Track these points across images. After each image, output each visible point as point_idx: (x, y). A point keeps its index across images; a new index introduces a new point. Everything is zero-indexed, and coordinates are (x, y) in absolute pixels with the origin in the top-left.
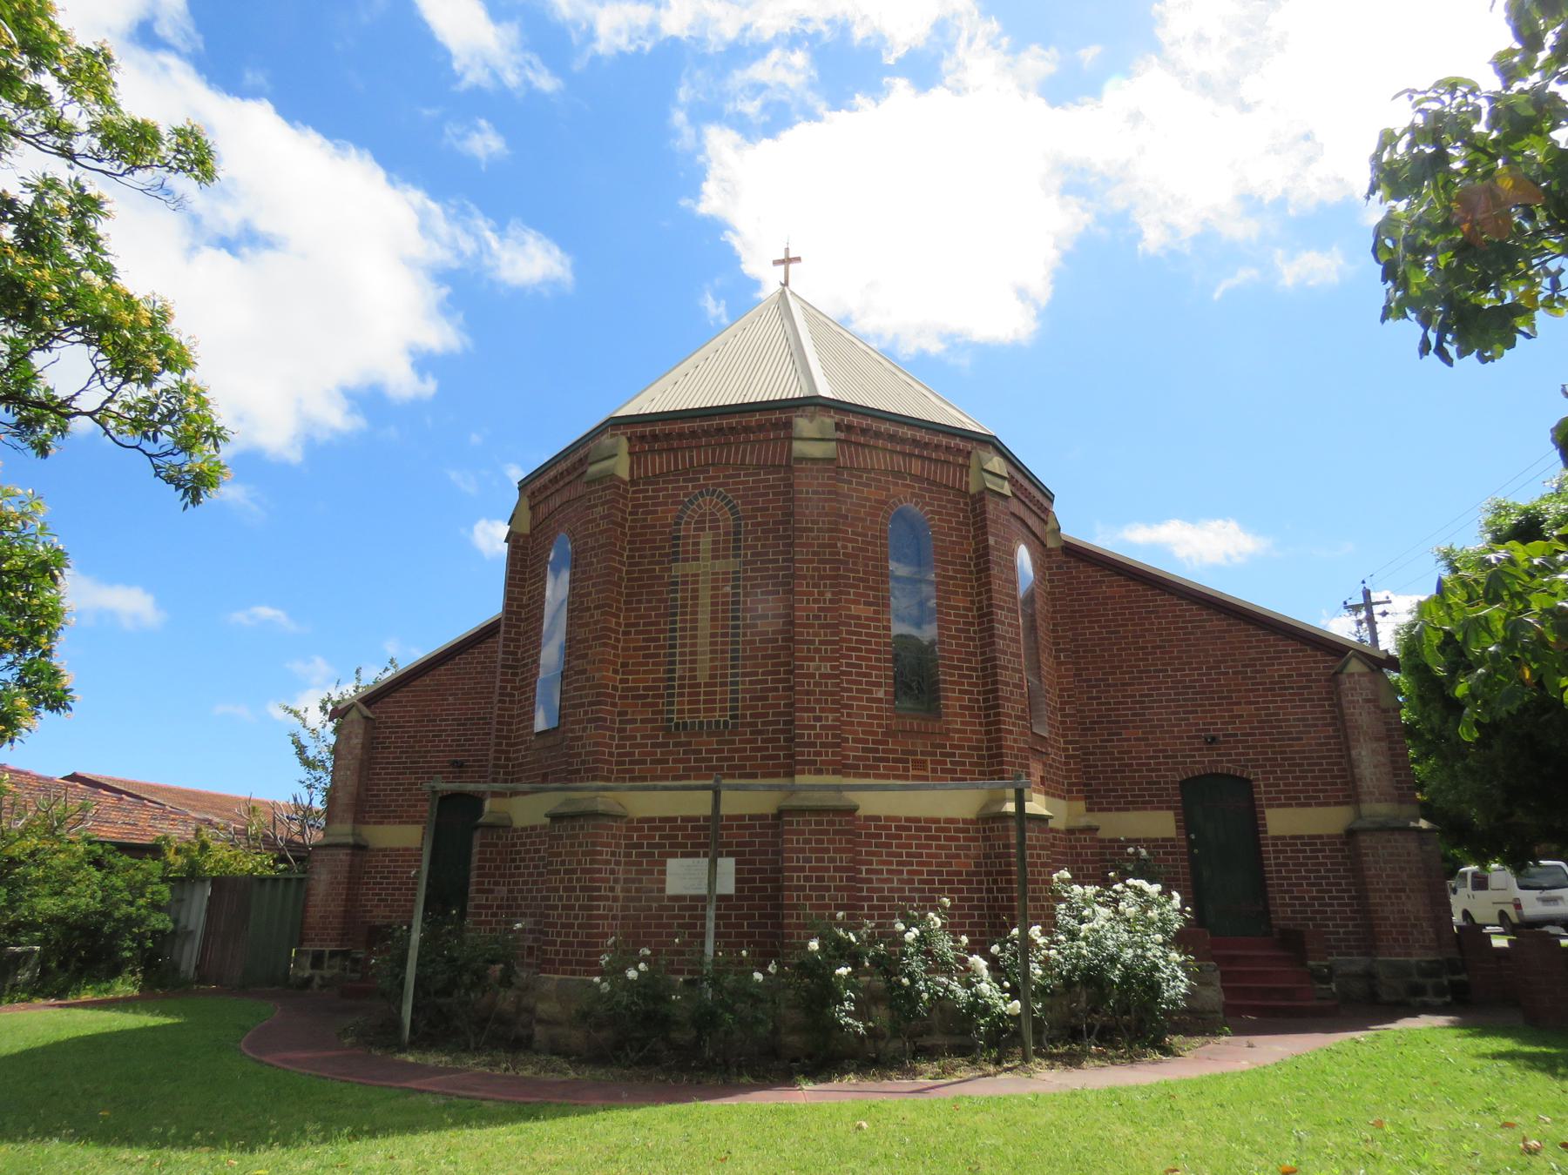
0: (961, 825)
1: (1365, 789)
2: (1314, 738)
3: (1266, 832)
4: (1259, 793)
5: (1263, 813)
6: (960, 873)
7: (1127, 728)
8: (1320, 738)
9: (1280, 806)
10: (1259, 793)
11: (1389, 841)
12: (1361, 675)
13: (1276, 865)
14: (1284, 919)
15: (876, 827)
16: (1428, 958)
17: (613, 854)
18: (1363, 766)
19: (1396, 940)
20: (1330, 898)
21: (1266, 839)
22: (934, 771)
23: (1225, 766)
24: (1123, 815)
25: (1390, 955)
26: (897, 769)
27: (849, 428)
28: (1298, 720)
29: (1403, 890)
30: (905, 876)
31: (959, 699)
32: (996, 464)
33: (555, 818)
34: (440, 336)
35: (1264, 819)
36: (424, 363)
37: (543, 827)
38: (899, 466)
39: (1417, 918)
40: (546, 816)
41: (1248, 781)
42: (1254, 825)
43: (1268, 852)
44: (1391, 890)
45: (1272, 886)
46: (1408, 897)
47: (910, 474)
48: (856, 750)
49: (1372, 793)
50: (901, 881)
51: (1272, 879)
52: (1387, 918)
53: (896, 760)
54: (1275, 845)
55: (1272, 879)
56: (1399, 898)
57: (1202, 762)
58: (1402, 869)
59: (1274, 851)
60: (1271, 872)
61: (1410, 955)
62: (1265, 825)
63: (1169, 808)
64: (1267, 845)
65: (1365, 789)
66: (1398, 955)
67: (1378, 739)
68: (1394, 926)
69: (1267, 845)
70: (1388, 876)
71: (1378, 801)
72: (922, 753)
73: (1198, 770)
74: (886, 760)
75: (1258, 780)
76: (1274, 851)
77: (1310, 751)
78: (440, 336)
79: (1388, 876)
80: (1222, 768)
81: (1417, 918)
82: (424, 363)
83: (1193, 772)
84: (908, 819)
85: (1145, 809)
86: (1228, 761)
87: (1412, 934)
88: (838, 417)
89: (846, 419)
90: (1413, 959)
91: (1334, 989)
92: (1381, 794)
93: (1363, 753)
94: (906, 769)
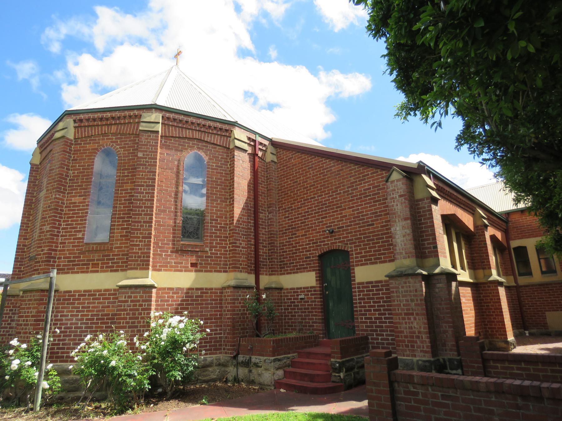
0: (112, 292)
1: (398, 251)
2: (380, 223)
3: (354, 280)
4: (353, 258)
5: (354, 269)
6: (108, 315)
7: (298, 230)
8: (383, 222)
9: (362, 265)
10: (353, 258)
11: (405, 283)
12: (398, 181)
13: (359, 299)
14: (362, 330)
15: (69, 296)
16: (424, 359)
17: (226, 300)
18: (397, 237)
19: (407, 346)
20: (365, 318)
21: (355, 284)
22: (102, 267)
23: (339, 245)
24: (296, 275)
25: (404, 356)
26: (84, 268)
27: (81, 121)
28: (373, 213)
29: (412, 314)
30: (79, 317)
31: (120, 233)
32: (156, 116)
33: (391, 277)
34: (329, 118)
35: (354, 273)
36: (327, 128)
37: (386, 281)
38: (105, 131)
39: (419, 332)
40: (386, 276)
41: (348, 252)
42: (349, 276)
43: (355, 292)
44: (405, 314)
45: (357, 311)
46: (415, 319)
47: (111, 133)
48: (65, 262)
49: (401, 253)
50: (77, 320)
51: (356, 307)
52: (402, 332)
53: (83, 265)
54: (359, 288)
55: (356, 307)
56: (409, 319)
57: (329, 244)
58: (412, 300)
59: (359, 292)
60: (356, 303)
61: (415, 356)
62: (354, 277)
63: (313, 270)
64: (355, 288)
65: (398, 251)
66: (408, 356)
67: (406, 219)
68: (406, 337)
69: (355, 288)
70: (404, 305)
71: (405, 258)
72: (97, 260)
73: (326, 249)
74: (79, 265)
75: (352, 251)
76: (359, 292)
77: (378, 231)
78: (329, 118)
79: (404, 305)
80: (336, 246)
81: (419, 332)
82: (327, 128)
83: (323, 250)
84: (85, 291)
85: (304, 272)
86: (339, 242)
87: (416, 342)
88: (74, 117)
89: (105, 115)
90: (415, 359)
91: (342, 377)
92: (406, 253)
93: (398, 229)
94: (88, 268)
